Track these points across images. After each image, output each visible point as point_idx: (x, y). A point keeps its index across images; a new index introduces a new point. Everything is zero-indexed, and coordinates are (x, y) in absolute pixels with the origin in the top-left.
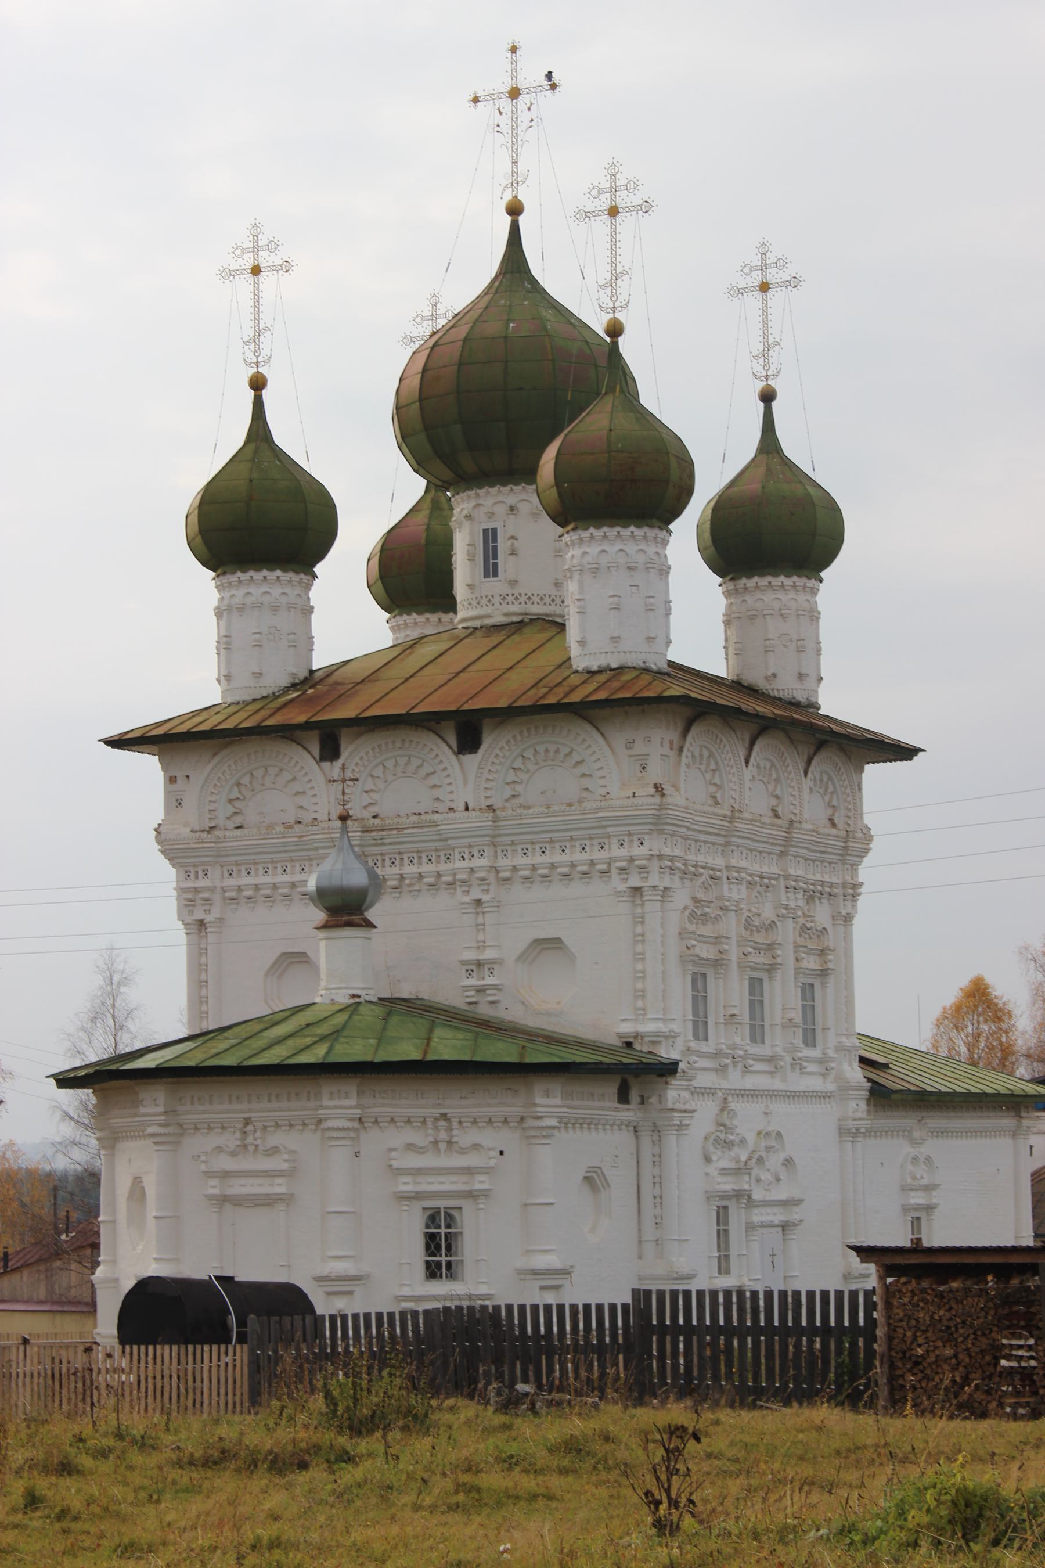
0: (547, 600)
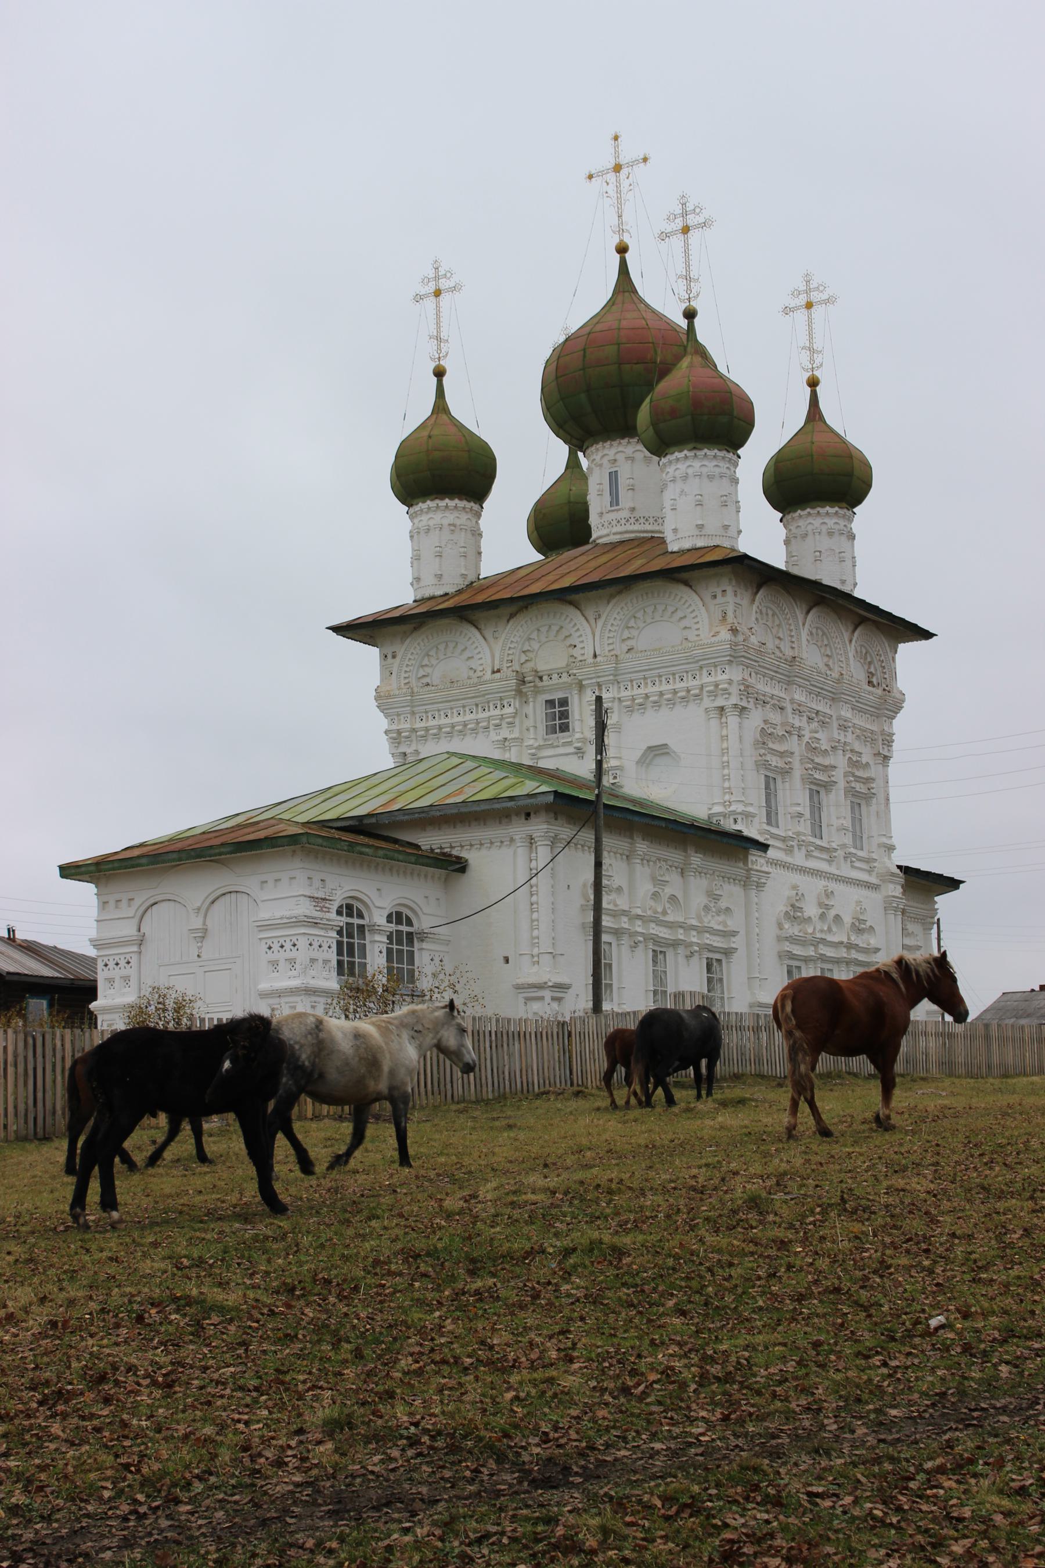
0: (651, 520)
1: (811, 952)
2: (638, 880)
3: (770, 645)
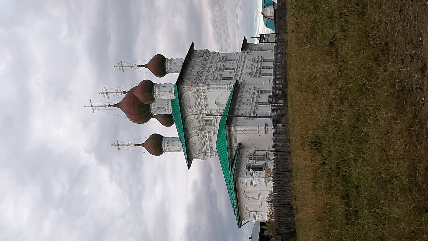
1: (259, 71)
2: (244, 108)
3: (195, 78)
